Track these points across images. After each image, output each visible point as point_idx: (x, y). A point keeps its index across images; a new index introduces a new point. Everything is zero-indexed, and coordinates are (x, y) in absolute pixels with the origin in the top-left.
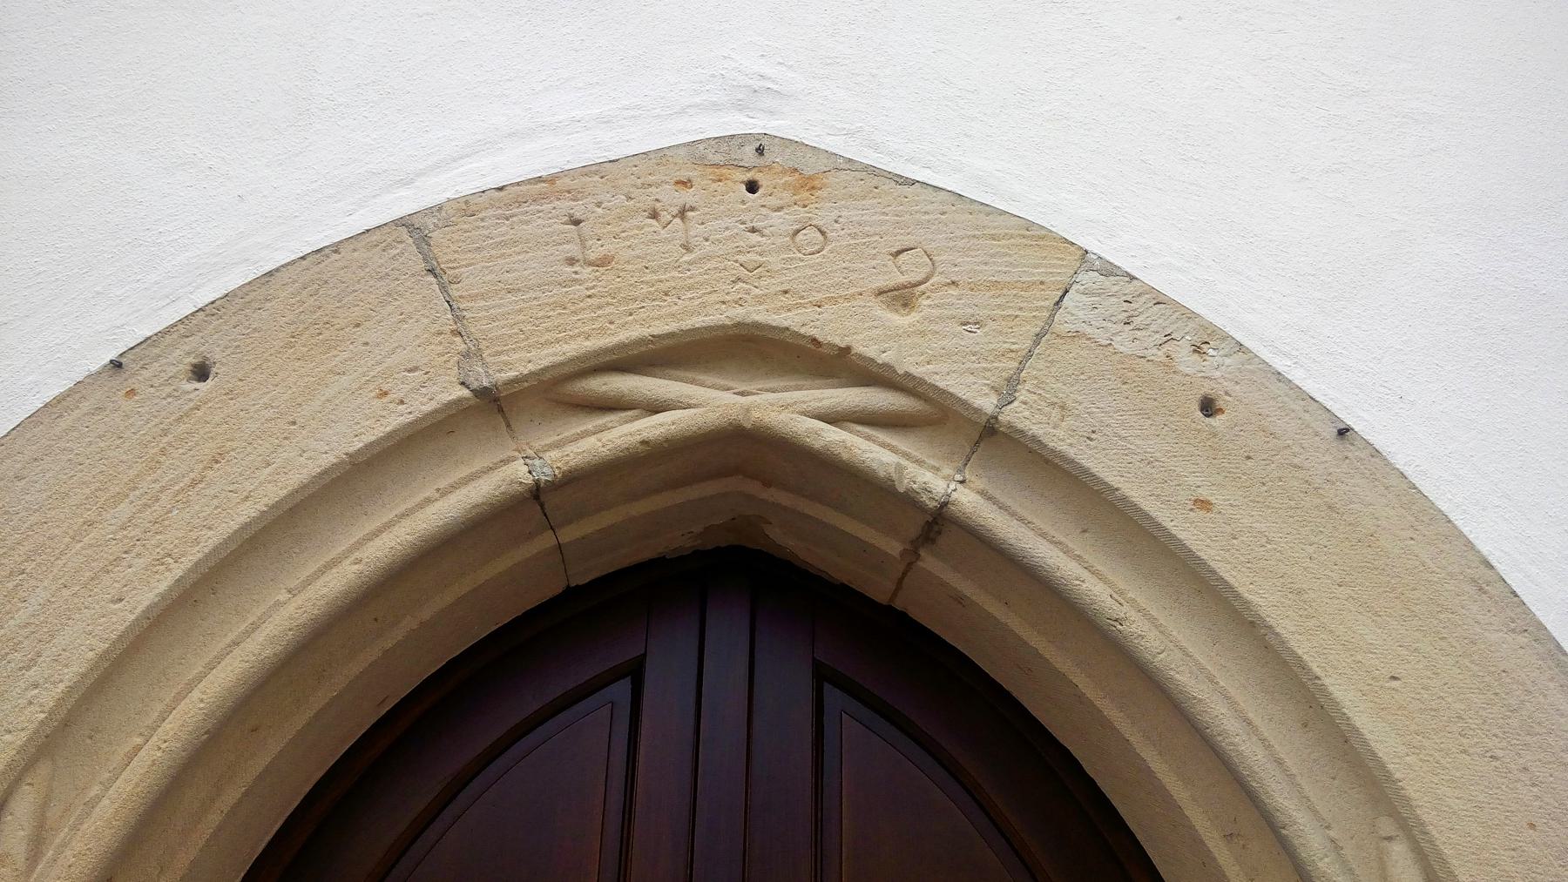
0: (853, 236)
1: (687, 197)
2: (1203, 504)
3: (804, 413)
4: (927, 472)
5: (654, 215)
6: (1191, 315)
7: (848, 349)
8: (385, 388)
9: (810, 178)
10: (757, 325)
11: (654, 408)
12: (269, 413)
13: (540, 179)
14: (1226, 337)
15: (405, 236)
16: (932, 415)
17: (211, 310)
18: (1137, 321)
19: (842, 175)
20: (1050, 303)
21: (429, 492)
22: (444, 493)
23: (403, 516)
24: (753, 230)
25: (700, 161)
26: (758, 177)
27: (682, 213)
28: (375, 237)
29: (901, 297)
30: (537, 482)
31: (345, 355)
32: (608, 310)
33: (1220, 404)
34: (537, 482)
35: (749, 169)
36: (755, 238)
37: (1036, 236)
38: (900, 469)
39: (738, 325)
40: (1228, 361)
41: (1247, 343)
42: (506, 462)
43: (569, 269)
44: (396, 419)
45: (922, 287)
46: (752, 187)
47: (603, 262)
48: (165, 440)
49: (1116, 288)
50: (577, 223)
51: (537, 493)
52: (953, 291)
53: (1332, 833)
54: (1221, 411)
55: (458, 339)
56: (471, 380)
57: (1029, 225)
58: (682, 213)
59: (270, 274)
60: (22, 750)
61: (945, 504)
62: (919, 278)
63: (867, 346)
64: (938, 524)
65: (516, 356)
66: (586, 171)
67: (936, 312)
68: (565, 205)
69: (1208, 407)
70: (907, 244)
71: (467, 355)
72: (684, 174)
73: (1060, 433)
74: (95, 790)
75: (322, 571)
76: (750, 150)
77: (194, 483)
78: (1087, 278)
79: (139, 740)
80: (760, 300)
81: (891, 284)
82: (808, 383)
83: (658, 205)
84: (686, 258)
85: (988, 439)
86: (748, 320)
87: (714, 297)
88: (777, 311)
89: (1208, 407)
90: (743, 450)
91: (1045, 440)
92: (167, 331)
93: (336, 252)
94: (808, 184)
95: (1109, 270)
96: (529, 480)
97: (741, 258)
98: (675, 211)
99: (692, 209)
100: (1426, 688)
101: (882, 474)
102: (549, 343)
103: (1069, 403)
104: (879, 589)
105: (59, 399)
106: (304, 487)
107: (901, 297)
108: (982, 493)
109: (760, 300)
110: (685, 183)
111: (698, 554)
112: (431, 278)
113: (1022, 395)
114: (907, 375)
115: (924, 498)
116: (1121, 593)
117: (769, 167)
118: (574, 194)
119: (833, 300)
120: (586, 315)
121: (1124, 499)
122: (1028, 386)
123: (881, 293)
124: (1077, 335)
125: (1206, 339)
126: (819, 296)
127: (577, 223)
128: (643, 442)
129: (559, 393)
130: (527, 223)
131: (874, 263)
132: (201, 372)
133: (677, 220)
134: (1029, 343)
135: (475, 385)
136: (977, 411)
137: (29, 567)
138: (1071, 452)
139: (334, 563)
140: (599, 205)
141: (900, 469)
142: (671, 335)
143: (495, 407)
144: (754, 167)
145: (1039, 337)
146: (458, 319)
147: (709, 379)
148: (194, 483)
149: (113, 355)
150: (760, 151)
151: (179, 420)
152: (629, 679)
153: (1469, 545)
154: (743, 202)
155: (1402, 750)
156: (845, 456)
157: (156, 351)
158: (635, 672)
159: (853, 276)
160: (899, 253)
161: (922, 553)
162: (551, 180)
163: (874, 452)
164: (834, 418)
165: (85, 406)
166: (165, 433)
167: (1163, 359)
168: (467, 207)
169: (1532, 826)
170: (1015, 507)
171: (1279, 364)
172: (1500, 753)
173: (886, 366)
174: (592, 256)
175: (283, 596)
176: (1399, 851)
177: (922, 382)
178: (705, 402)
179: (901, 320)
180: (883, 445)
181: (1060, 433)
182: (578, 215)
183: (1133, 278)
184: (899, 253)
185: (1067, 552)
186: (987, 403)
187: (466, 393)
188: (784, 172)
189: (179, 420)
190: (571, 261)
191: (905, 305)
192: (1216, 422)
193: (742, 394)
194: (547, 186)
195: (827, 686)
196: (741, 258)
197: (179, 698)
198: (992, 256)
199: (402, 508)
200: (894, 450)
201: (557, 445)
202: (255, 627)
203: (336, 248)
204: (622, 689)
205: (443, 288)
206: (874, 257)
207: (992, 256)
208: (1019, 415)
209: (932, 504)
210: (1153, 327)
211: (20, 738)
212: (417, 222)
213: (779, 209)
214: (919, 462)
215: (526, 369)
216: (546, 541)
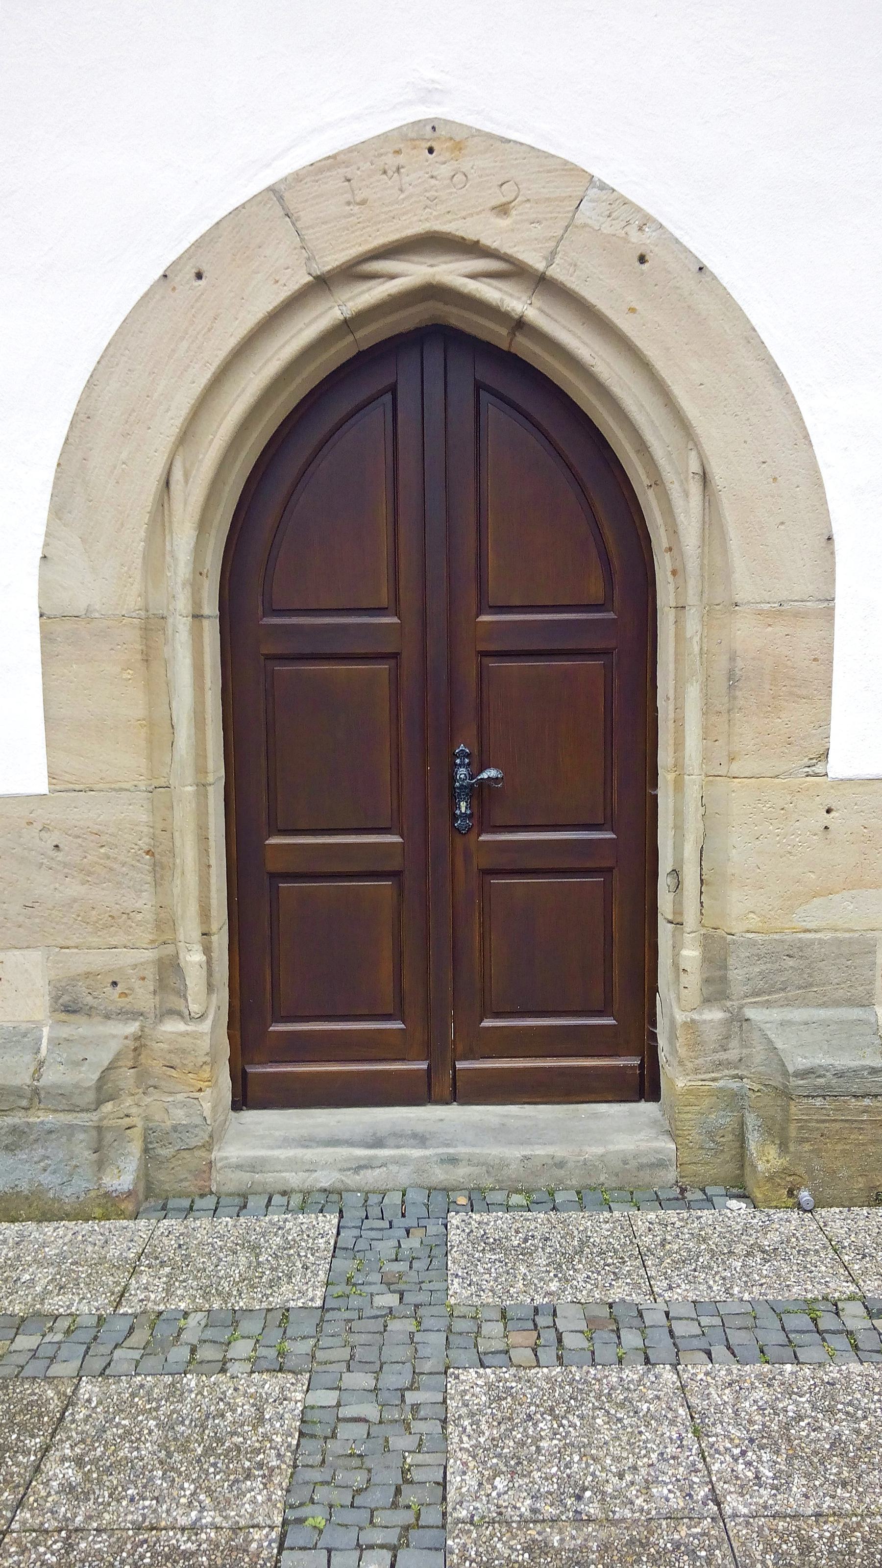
0: (481, 176)
1: (401, 159)
2: (632, 310)
3: (459, 275)
4: (515, 301)
5: (385, 172)
6: (639, 210)
7: (478, 242)
8: (277, 278)
9: (459, 142)
10: (436, 232)
11: (392, 277)
12: (232, 294)
13: (329, 157)
14: (654, 221)
15: (272, 196)
16: (515, 271)
17: (197, 245)
18: (614, 215)
19: (475, 139)
20: (573, 208)
21: (301, 325)
22: (307, 325)
23: (292, 337)
24: (432, 177)
25: (405, 138)
26: (434, 145)
27: (398, 169)
28: (260, 198)
29: (503, 210)
30: (345, 318)
31: (257, 263)
32: (369, 229)
33: (647, 258)
34: (345, 318)
35: (429, 140)
36: (433, 182)
37: (570, 170)
38: (502, 300)
39: (427, 233)
40: (654, 234)
41: (664, 224)
42: (331, 308)
43: (348, 208)
44: (284, 294)
45: (513, 204)
46: (431, 151)
47: (363, 202)
48: (193, 310)
49: (605, 197)
50: (349, 180)
51: (346, 321)
52: (528, 205)
53: (669, 449)
54: (647, 261)
55: (303, 251)
56: (312, 272)
57: (566, 163)
58: (398, 169)
59: (217, 223)
60: (174, 443)
61: (521, 317)
62: (512, 199)
63: (488, 240)
64: (520, 325)
65: (330, 258)
66: (350, 150)
67: (519, 218)
68: (342, 171)
69: (642, 259)
70: (506, 179)
71: (308, 259)
72: (396, 148)
73: (573, 279)
74: (201, 456)
75: (265, 364)
76: (429, 128)
77: (209, 330)
78: (593, 193)
79: (211, 437)
80: (437, 218)
81: (499, 203)
82: (461, 257)
83: (386, 167)
84: (402, 196)
85: (542, 283)
86: (432, 230)
87: (415, 218)
88: (445, 223)
89: (642, 259)
90: (432, 292)
91: (565, 283)
92: (180, 258)
93: (244, 208)
94: (458, 147)
95: (603, 187)
96: (342, 318)
97: (427, 194)
98: (395, 169)
99: (403, 167)
100: (714, 388)
101: (494, 304)
102: (343, 250)
103: (579, 263)
104: (504, 346)
105: (146, 294)
106: (252, 329)
107: (503, 210)
108: (541, 310)
109: (437, 218)
110: (398, 152)
111: (417, 330)
112: (287, 219)
113: (557, 261)
114: (505, 254)
115: (513, 314)
116: (596, 353)
117: (439, 138)
118: (347, 164)
119: (471, 215)
120: (358, 233)
121: (599, 310)
122: (560, 255)
123: (493, 208)
124: (585, 225)
125: (646, 221)
126: (464, 214)
127: (349, 180)
128: (389, 295)
129: (352, 273)
130: (326, 183)
131: (490, 192)
132: (199, 276)
133: (396, 174)
134: (562, 232)
135: (314, 275)
136: (536, 270)
137: (156, 370)
138: (577, 289)
139: (269, 360)
140: (358, 169)
141: (502, 300)
142: (397, 241)
143: (323, 284)
144: (432, 140)
145: (567, 227)
146: (302, 240)
147: (416, 258)
148: (209, 330)
149: (161, 273)
150: (434, 128)
151: (197, 301)
152: (390, 393)
153: (748, 321)
154: (427, 161)
155: (699, 415)
156: (478, 296)
157: (179, 267)
158: (393, 389)
159: (480, 200)
160: (502, 185)
161: (517, 334)
162: (334, 157)
163: (489, 292)
164: (473, 276)
165: (158, 297)
166: (192, 307)
167: (624, 235)
168: (298, 177)
169: (745, 442)
170: (555, 316)
171: (678, 234)
172: (739, 413)
173: (496, 250)
174: (358, 200)
175: (252, 376)
176: (693, 454)
177: (511, 257)
178: (415, 272)
179: (504, 223)
180: (496, 288)
181: (573, 279)
182: (349, 177)
183: (614, 190)
184: (502, 185)
185: (574, 334)
186: (540, 266)
187: (311, 278)
188: (446, 140)
189: (197, 301)
190: (349, 203)
191: (505, 214)
192: (645, 267)
193: (431, 266)
194: (334, 161)
195: (482, 392)
196: (427, 194)
197: (223, 419)
198: (548, 182)
199: (292, 333)
200: (500, 290)
201: (350, 299)
202: (244, 390)
203: (243, 206)
204: (388, 397)
205: (293, 224)
206: (490, 188)
207: (548, 182)
208: (556, 272)
209: (516, 317)
210: (621, 218)
211: (173, 439)
212: (276, 188)
213: (444, 163)
214: (511, 295)
215: (337, 263)
216: (350, 338)
